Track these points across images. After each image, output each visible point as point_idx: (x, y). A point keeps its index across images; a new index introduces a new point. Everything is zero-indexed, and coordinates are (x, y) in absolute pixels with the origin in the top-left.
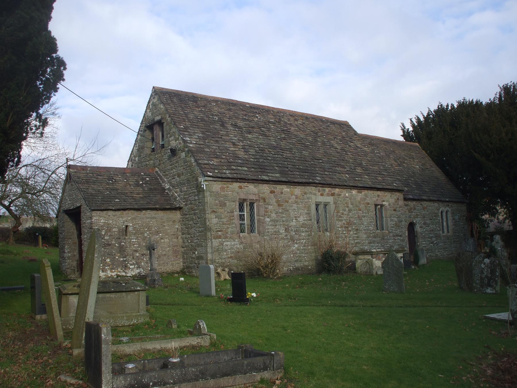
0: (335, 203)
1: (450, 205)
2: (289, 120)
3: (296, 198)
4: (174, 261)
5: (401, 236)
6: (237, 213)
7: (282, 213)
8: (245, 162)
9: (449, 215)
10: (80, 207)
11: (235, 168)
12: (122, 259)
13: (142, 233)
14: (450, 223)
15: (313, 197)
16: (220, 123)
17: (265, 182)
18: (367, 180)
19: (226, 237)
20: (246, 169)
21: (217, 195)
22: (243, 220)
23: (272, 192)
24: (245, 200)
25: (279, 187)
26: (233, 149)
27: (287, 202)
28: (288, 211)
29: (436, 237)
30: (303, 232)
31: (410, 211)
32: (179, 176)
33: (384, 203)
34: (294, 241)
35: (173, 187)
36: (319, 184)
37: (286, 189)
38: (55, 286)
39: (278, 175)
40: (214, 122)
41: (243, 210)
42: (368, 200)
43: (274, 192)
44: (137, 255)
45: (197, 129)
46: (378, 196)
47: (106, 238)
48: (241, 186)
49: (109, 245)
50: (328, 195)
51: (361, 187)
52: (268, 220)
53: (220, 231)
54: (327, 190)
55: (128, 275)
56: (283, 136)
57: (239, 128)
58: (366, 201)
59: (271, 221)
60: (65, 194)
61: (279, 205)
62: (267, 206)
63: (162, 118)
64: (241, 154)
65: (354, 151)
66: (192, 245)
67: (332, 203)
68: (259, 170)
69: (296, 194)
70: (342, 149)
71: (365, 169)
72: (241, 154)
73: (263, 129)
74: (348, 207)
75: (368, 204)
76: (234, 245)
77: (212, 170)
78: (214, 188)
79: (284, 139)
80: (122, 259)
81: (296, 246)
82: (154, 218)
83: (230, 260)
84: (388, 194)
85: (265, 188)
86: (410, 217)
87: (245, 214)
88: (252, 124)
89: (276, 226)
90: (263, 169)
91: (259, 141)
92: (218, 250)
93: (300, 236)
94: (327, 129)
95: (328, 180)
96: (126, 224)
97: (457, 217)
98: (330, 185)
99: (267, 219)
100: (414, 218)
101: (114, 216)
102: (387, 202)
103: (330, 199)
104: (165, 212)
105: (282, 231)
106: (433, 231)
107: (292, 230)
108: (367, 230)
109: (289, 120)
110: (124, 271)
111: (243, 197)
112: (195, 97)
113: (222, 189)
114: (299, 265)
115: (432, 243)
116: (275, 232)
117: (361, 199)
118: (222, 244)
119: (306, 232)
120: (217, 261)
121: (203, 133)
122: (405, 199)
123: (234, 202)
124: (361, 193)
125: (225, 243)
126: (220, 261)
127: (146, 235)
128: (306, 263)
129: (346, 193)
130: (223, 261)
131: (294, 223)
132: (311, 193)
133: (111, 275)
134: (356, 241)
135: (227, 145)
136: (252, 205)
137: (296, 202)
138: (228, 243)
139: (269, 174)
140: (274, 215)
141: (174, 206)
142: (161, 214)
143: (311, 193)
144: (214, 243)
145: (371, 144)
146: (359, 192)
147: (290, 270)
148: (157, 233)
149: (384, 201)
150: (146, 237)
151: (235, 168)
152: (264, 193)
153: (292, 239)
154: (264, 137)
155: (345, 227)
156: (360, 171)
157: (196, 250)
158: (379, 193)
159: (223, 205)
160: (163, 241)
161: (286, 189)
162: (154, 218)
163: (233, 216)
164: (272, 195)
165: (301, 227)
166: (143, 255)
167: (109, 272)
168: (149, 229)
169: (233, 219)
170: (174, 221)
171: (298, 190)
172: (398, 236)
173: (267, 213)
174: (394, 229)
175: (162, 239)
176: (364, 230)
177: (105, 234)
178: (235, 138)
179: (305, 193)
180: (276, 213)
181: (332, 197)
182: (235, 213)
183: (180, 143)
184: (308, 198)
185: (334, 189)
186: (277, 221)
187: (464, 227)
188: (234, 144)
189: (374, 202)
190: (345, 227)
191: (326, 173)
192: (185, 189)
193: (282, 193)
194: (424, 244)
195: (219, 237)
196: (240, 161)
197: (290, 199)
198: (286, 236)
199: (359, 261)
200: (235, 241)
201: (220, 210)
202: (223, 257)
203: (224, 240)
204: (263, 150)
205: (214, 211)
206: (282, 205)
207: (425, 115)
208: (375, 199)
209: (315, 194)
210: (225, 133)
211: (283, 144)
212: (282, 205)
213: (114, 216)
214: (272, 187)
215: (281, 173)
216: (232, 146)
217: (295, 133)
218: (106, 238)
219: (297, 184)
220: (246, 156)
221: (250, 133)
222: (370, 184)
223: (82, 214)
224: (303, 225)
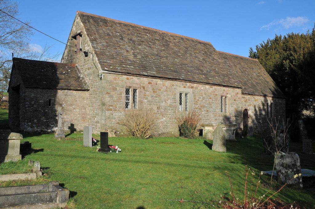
2: (169, 39)
3: (167, 88)
4: (82, 123)
6: (124, 95)
7: (156, 97)
8: (133, 63)
10: (19, 86)
11: (125, 66)
12: (45, 120)
14: (273, 111)
15: (178, 88)
16: (121, 37)
18: (217, 80)
19: (116, 110)
20: (132, 67)
21: (111, 83)
22: (129, 100)
23: (149, 83)
25: (155, 80)
26: (126, 54)
28: (160, 96)
31: (246, 101)
32: (89, 69)
33: (228, 95)
34: (163, 115)
35: (85, 76)
36: (183, 80)
38: (83, 134)
39: (154, 73)
40: (116, 36)
41: (129, 93)
43: (151, 83)
45: (103, 40)
46: (224, 90)
47: (34, 106)
48: (128, 78)
49: (37, 111)
50: (189, 87)
51: (212, 84)
53: (111, 106)
54: (188, 84)
56: (163, 48)
57: (134, 42)
58: (215, 93)
60: (13, 77)
63: (81, 32)
64: (131, 57)
65: (212, 61)
66: (93, 114)
67: (191, 93)
68: (142, 68)
69: (166, 85)
70: (204, 59)
71: (217, 73)
72: (131, 57)
73: (149, 43)
75: (217, 95)
77: (107, 66)
79: (164, 50)
80: (45, 120)
81: (164, 119)
83: (118, 125)
84: (230, 89)
85: (145, 80)
86: (245, 105)
88: (143, 40)
90: (145, 68)
91: (146, 51)
92: (109, 118)
93: (167, 112)
94: (195, 46)
96: (49, 98)
97: (278, 108)
98: (190, 81)
99: (145, 100)
100: (248, 106)
103: (190, 90)
108: (215, 111)
109: (169, 39)
110: (46, 128)
111: (129, 85)
112: (105, 20)
114: (166, 131)
117: (212, 91)
118: (112, 114)
121: (107, 43)
122: (243, 93)
128: (171, 130)
130: (113, 125)
131: (163, 104)
132: (177, 85)
133: (37, 130)
134: (206, 118)
135: (122, 51)
136: (135, 91)
137: (166, 91)
139: (148, 72)
140: (150, 98)
141: (84, 89)
143: (177, 85)
145: (225, 58)
148: (71, 105)
149: (228, 94)
151: (125, 66)
152: (144, 83)
154: (150, 48)
156: (213, 74)
157: (95, 117)
158: (225, 88)
159: (114, 89)
160: (75, 110)
161: (159, 81)
164: (150, 85)
167: (35, 128)
169: (121, 99)
171: (168, 83)
175: (74, 109)
177: (34, 104)
178: (128, 48)
179: (173, 85)
181: (192, 89)
183: (90, 48)
184: (175, 89)
185: (193, 84)
187: (282, 114)
188: (127, 51)
191: (189, 73)
192: (91, 78)
193: (157, 84)
195: (111, 110)
196: (129, 62)
197: (162, 88)
198: (158, 112)
204: (147, 56)
205: (108, 93)
206: (156, 92)
207: (266, 43)
209: (180, 87)
210: (122, 44)
211: (162, 54)
212: (156, 92)
214: (150, 79)
216: (126, 52)
217: (173, 47)
218: (34, 106)
219: (167, 79)
220: (135, 60)
221: (140, 45)
222: (218, 82)
223: (20, 90)
224: (170, 106)
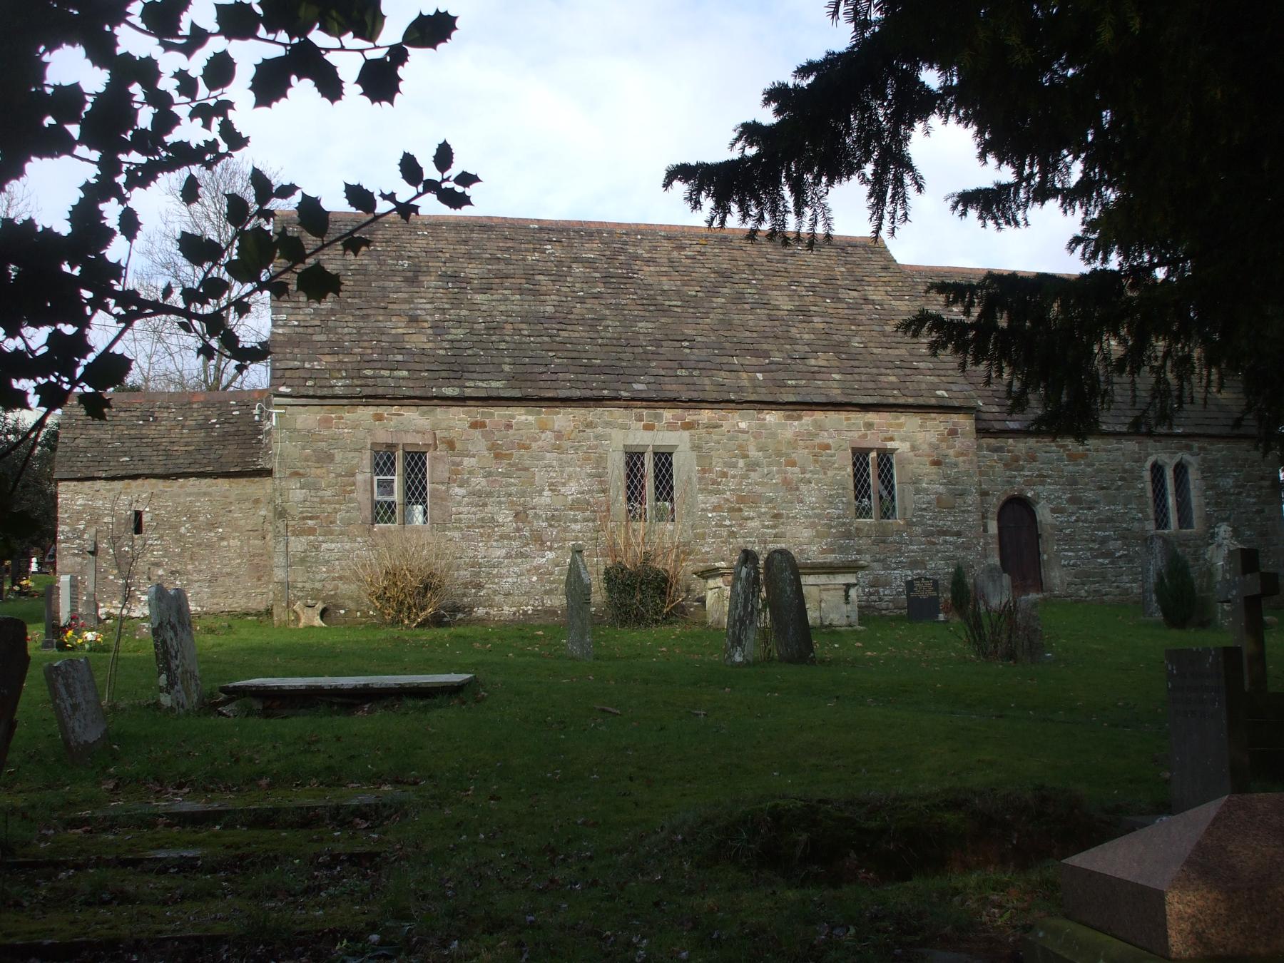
0: (696, 448)
1: (1196, 445)
4: (251, 588)
5: (958, 534)
9: (1193, 476)
13: (175, 527)
17: (450, 403)
20: (405, 373)
21: (308, 437)
24: (391, 447)
27: (527, 448)
28: (526, 469)
29: (1124, 538)
30: (576, 521)
37: (523, 418)
42: (824, 438)
43: (483, 425)
44: (160, 572)
46: (869, 426)
50: (671, 427)
52: (462, 491)
53: (311, 518)
54: (668, 415)
55: (133, 615)
58: (817, 441)
59: (469, 494)
61: (497, 456)
62: (458, 459)
69: (556, 428)
74: (745, 456)
76: (352, 550)
78: (299, 421)
81: (550, 555)
82: (205, 494)
83: (340, 584)
85: (457, 418)
87: (396, 478)
89: (485, 505)
92: (303, 561)
95: (672, 389)
97: (1227, 483)
98: (673, 402)
99: (457, 490)
100: (1029, 483)
101: (109, 491)
102: (902, 440)
104: (236, 480)
105: (505, 517)
106: (1110, 520)
107: (537, 516)
111: (383, 437)
113: (326, 422)
115: (1108, 554)
116: (482, 520)
118: (317, 548)
119: (585, 520)
120: (300, 585)
122: (978, 431)
123: (359, 450)
124: (799, 418)
125: (324, 546)
126: (308, 585)
127: (183, 530)
129: (742, 421)
130: (318, 585)
131: (546, 498)
137: (557, 448)
138: (331, 547)
142: (223, 483)
143: (608, 424)
144: (291, 545)
146: (788, 418)
147: (525, 613)
148: (212, 526)
149: (892, 439)
150: (182, 536)
153: (539, 539)
155: (731, 510)
158: (871, 417)
159: (325, 458)
160: (225, 543)
161: (522, 416)
162: (205, 494)
163: (354, 484)
164: (477, 433)
165: (571, 509)
166: (173, 573)
168: (192, 517)
169: (352, 492)
170: (257, 501)
171: (563, 419)
172: (945, 533)
173: (456, 476)
174: (928, 515)
175: (223, 539)
176: (805, 517)
179: (590, 425)
180: (488, 475)
181: (686, 434)
182: (359, 477)
184: (597, 437)
186: (489, 495)
189: (852, 441)
190: (731, 510)
193: (509, 426)
194: (1070, 558)
195: (311, 531)
197: (535, 440)
198: (518, 529)
199: (710, 593)
200: (353, 540)
201: (313, 470)
202: (318, 577)
203: (321, 538)
205: (296, 474)
208: (856, 435)
213: (109, 491)
214: (478, 413)
215: (512, 378)
224: (577, 505)
